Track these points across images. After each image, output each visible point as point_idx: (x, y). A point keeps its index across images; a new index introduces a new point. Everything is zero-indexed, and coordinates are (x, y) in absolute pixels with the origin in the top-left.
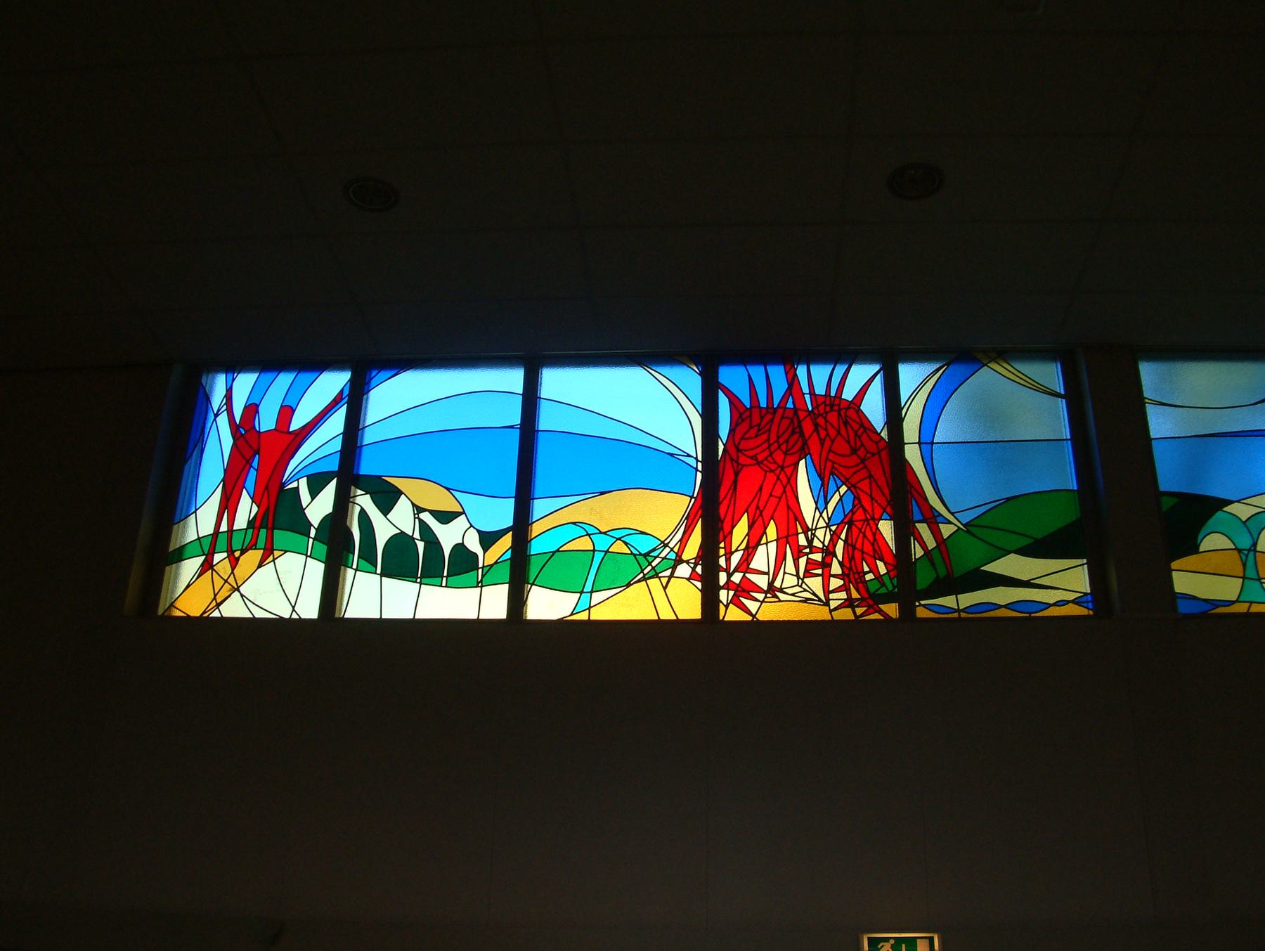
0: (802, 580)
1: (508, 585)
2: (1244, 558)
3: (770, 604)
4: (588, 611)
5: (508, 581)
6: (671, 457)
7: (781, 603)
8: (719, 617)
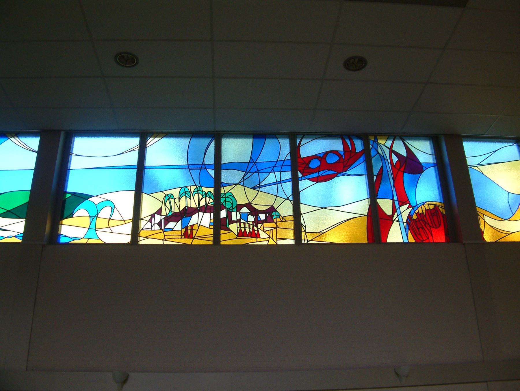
0: (270, 237)
1: (403, 242)
2: (91, 220)
3: (234, 188)
4: (281, 167)
5: (404, 242)
6: (197, 240)
7: (228, 191)
8: (482, 231)
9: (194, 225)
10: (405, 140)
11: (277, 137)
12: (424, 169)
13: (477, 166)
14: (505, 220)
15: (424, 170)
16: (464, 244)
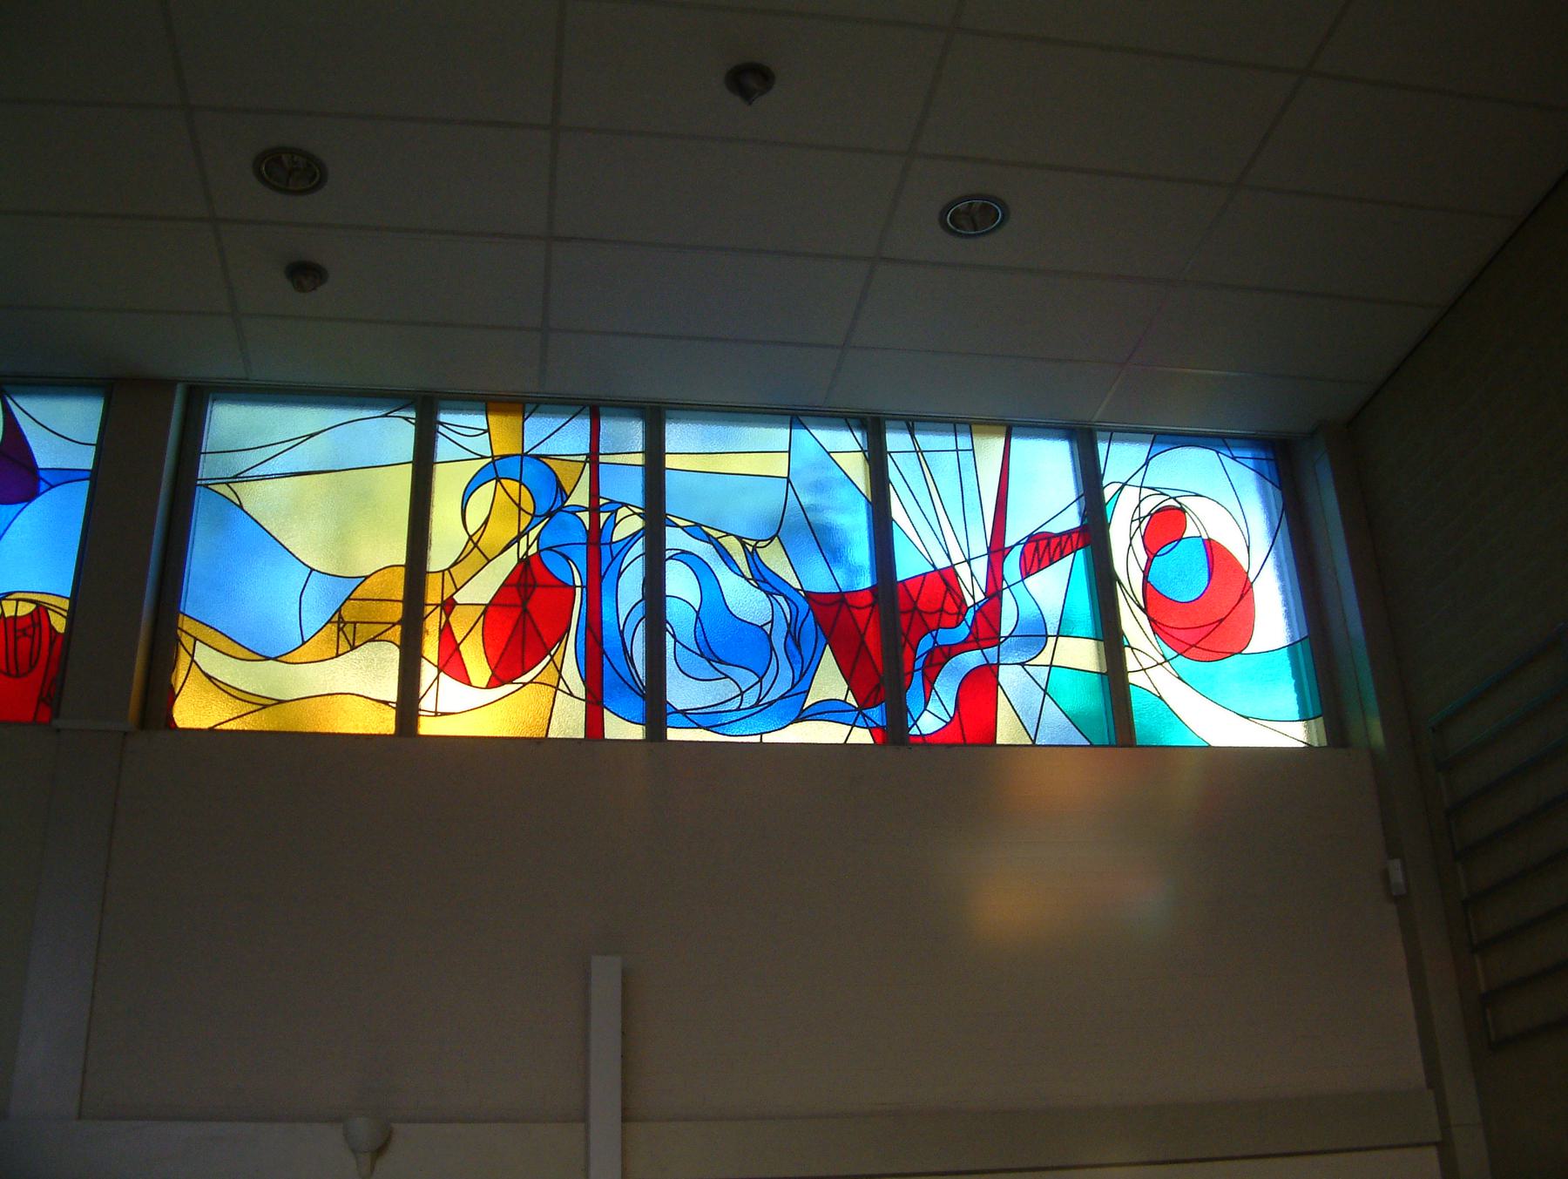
9: (484, 686)
10: (12, 396)
11: (1229, 444)
12: (43, 486)
13: (227, 484)
14: (267, 658)
15: (42, 491)
16: (58, 730)
